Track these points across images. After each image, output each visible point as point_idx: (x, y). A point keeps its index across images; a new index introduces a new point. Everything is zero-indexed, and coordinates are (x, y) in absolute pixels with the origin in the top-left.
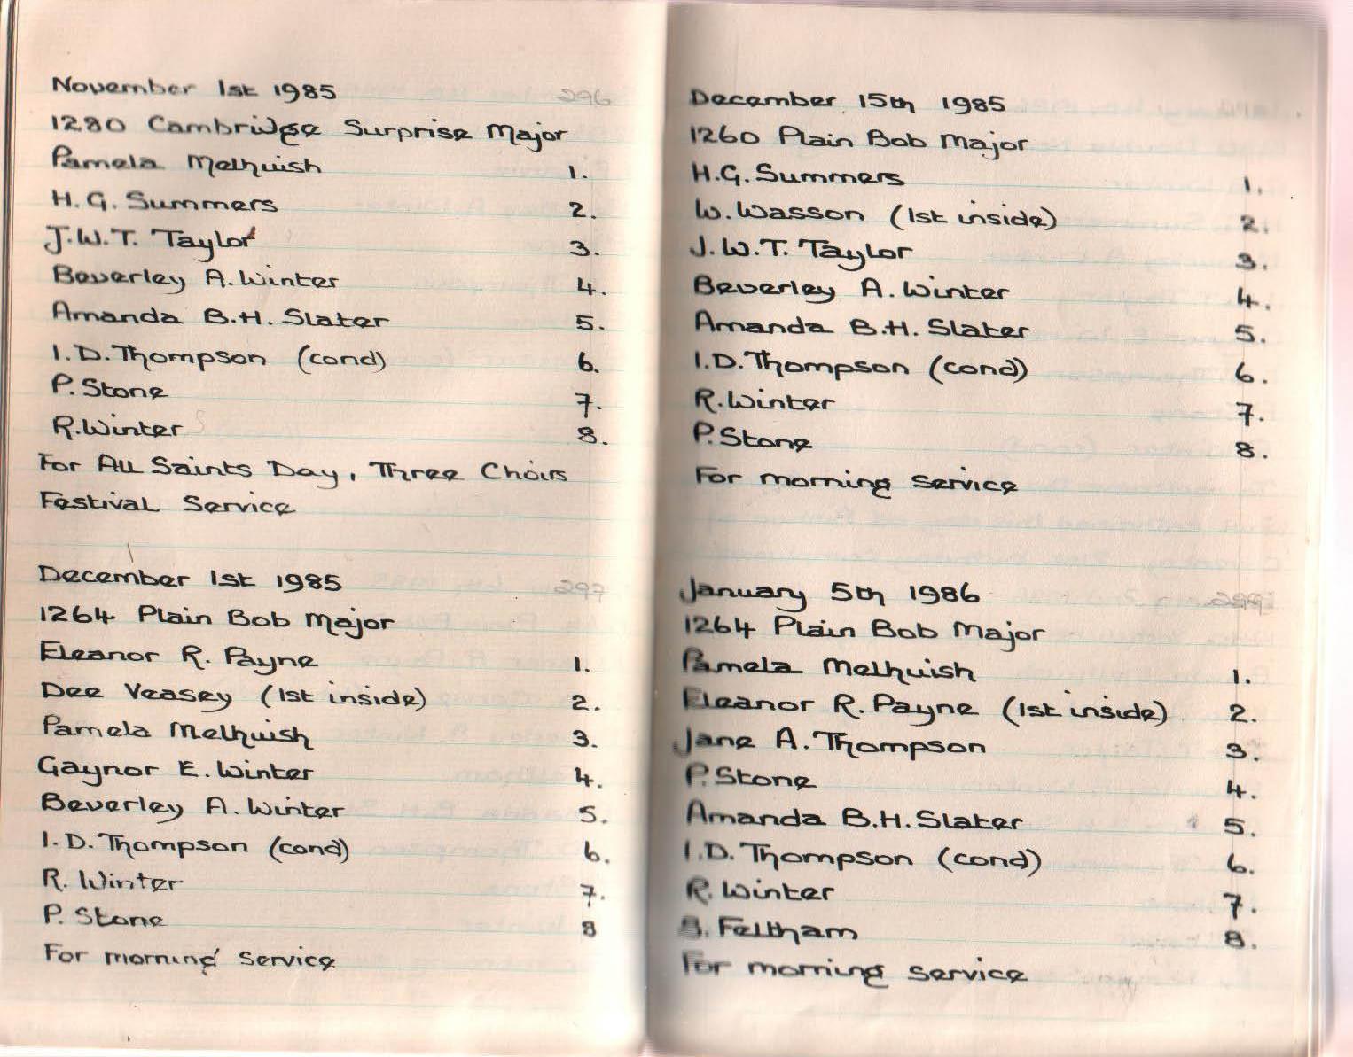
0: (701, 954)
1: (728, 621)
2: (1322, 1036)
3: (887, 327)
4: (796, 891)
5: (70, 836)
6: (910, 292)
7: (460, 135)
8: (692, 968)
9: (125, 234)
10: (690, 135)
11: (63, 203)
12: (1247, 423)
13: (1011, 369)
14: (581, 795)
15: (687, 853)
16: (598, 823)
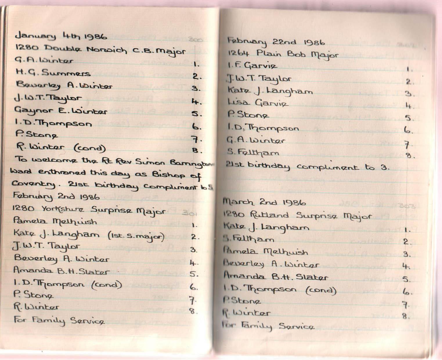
0: (228, 321)
1: (241, 51)
2: (434, 348)
3: (283, 277)
4: (97, 111)
5: (24, 280)
6: (32, 147)
7: (129, 211)
8: (225, 326)
9: (39, 244)
10: (228, 53)
11: (20, 73)
12: (196, 142)
13: (120, 50)
14: (191, 268)
15: (225, 289)
16: (196, 276)
